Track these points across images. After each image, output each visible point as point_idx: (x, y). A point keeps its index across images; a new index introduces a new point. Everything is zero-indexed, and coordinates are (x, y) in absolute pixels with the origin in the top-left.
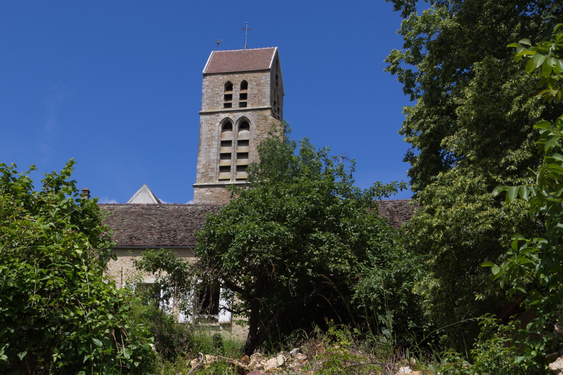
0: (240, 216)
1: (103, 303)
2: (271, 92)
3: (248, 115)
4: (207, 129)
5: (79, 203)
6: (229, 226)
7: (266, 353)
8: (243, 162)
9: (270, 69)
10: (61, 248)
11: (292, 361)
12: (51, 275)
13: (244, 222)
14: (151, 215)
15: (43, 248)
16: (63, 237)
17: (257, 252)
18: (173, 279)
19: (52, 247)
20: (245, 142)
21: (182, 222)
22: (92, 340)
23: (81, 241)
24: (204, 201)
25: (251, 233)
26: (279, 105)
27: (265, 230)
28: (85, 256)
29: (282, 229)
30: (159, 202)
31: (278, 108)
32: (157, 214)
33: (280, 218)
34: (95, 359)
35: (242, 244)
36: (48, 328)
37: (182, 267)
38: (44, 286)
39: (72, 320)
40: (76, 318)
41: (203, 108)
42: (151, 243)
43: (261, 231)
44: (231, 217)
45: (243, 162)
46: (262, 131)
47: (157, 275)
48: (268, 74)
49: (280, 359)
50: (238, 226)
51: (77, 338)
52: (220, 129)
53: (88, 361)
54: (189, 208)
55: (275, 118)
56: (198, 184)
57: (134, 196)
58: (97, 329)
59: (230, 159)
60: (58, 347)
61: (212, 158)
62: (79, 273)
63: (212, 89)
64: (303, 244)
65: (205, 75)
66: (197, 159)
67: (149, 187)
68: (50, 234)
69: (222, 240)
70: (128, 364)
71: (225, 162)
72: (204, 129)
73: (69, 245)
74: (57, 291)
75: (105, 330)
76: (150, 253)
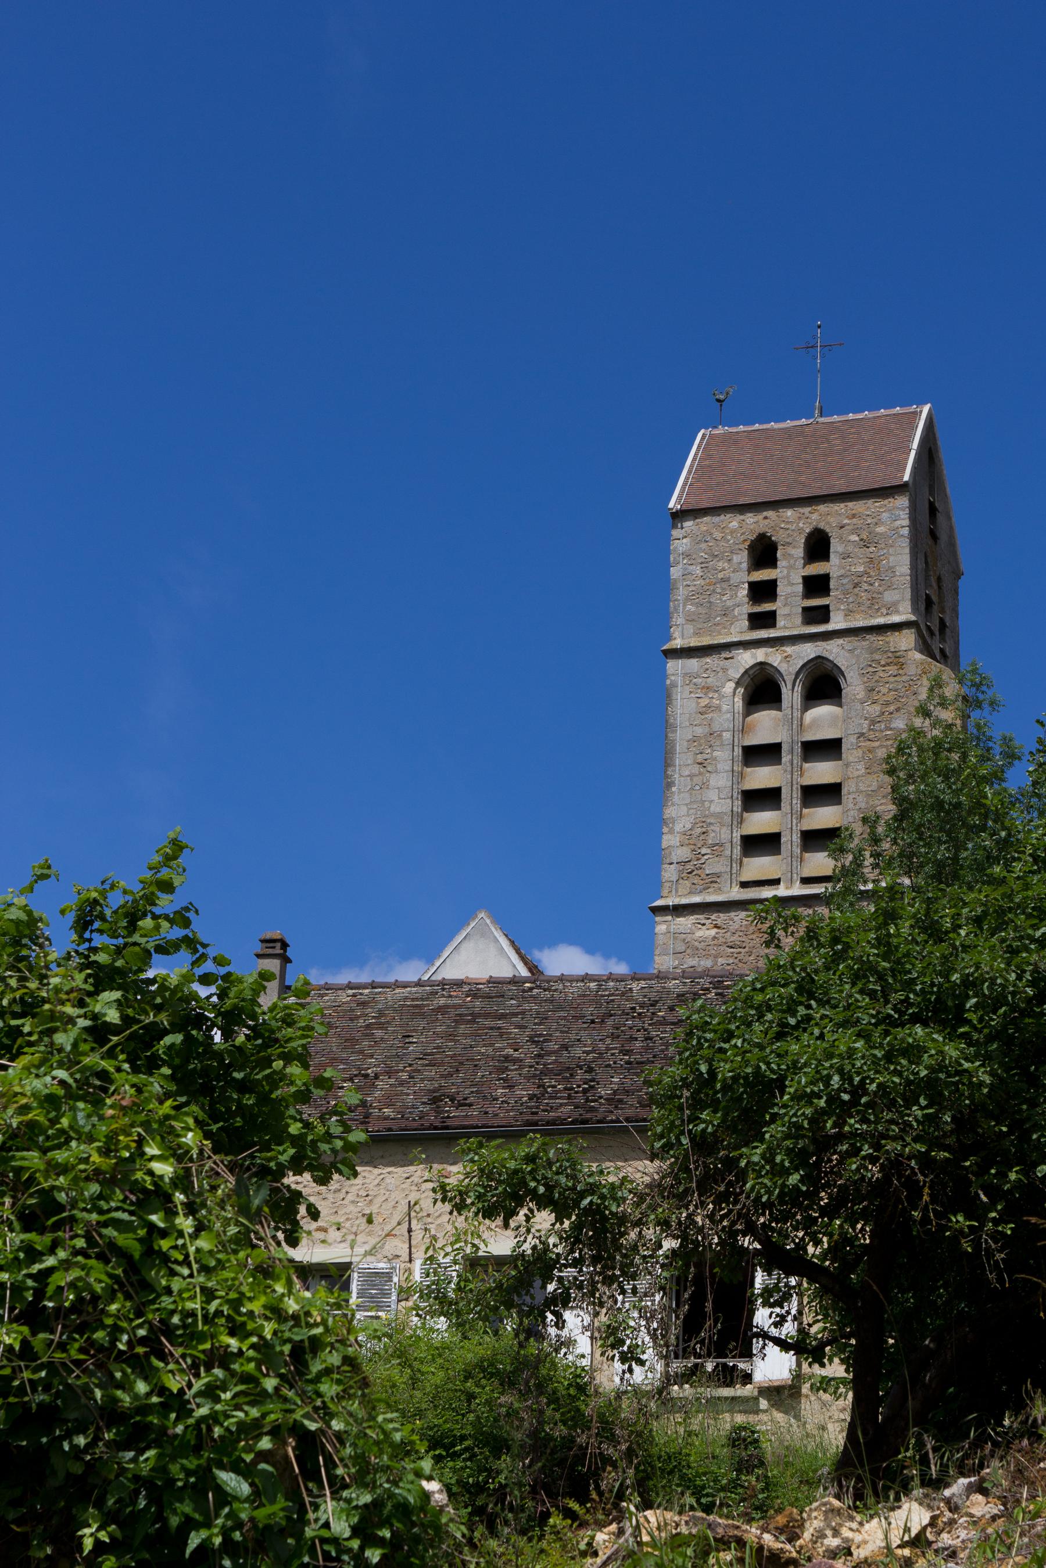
0: (802, 1011)
1: (253, 1346)
2: (914, 567)
3: (835, 651)
4: (691, 706)
5: (213, 989)
6: (761, 1047)
7: (858, 1496)
8: (823, 817)
9: (905, 485)
10: (95, 1158)
11: (952, 1522)
12: (62, 1254)
13: (817, 1032)
14: (502, 1017)
15: (32, 1159)
16: (101, 1118)
17: (863, 1136)
18: (577, 1241)
19: (60, 1156)
20: (827, 748)
21: (614, 1037)
22: (214, 1478)
23: (172, 1131)
24: (691, 962)
25: (840, 1071)
26: (942, 611)
27: (889, 1057)
28: (183, 1181)
29: (952, 1051)
30: (533, 968)
31: (942, 622)
32: (523, 1013)
33: (943, 1012)
34: (227, 1540)
35: (808, 1111)
36: (62, 1438)
37: (603, 1197)
38: (40, 1294)
39: (144, 1409)
40: (155, 1399)
41: (676, 632)
42: (504, 1115)
43: (876, 1061)
44: (769, 1017)
45: (823, 817)
46: (887, 704)
47: (518, 1228)
48: (902, 502)
49: (913, 1514)
50: (795, 1047)
51: (160, 1469)
52: (739, 703)
53: (204, 1548)
54: (635, 986)
55: (932, 656)
56: (670, 902)
57: (446, 954)
58: (230, 1440)
59: (779, 808)
60: (99, 1504)
61: (715, 808)
62: (165, 1244)
63: (704, 565)
64: (1025, 1101)
65: (679, 516)
66: (662, 813)
67: (497, 920)
68: (57, 1109)
69: (740, 1099)
70: (346, 1558)
71: (762, 821)
72: (683, 706)
73: (127, 1148)
74: (86, 1311)
75: (258, 1437)
76: (492, 1153)
